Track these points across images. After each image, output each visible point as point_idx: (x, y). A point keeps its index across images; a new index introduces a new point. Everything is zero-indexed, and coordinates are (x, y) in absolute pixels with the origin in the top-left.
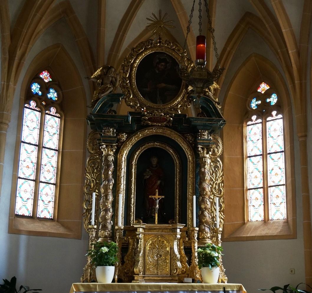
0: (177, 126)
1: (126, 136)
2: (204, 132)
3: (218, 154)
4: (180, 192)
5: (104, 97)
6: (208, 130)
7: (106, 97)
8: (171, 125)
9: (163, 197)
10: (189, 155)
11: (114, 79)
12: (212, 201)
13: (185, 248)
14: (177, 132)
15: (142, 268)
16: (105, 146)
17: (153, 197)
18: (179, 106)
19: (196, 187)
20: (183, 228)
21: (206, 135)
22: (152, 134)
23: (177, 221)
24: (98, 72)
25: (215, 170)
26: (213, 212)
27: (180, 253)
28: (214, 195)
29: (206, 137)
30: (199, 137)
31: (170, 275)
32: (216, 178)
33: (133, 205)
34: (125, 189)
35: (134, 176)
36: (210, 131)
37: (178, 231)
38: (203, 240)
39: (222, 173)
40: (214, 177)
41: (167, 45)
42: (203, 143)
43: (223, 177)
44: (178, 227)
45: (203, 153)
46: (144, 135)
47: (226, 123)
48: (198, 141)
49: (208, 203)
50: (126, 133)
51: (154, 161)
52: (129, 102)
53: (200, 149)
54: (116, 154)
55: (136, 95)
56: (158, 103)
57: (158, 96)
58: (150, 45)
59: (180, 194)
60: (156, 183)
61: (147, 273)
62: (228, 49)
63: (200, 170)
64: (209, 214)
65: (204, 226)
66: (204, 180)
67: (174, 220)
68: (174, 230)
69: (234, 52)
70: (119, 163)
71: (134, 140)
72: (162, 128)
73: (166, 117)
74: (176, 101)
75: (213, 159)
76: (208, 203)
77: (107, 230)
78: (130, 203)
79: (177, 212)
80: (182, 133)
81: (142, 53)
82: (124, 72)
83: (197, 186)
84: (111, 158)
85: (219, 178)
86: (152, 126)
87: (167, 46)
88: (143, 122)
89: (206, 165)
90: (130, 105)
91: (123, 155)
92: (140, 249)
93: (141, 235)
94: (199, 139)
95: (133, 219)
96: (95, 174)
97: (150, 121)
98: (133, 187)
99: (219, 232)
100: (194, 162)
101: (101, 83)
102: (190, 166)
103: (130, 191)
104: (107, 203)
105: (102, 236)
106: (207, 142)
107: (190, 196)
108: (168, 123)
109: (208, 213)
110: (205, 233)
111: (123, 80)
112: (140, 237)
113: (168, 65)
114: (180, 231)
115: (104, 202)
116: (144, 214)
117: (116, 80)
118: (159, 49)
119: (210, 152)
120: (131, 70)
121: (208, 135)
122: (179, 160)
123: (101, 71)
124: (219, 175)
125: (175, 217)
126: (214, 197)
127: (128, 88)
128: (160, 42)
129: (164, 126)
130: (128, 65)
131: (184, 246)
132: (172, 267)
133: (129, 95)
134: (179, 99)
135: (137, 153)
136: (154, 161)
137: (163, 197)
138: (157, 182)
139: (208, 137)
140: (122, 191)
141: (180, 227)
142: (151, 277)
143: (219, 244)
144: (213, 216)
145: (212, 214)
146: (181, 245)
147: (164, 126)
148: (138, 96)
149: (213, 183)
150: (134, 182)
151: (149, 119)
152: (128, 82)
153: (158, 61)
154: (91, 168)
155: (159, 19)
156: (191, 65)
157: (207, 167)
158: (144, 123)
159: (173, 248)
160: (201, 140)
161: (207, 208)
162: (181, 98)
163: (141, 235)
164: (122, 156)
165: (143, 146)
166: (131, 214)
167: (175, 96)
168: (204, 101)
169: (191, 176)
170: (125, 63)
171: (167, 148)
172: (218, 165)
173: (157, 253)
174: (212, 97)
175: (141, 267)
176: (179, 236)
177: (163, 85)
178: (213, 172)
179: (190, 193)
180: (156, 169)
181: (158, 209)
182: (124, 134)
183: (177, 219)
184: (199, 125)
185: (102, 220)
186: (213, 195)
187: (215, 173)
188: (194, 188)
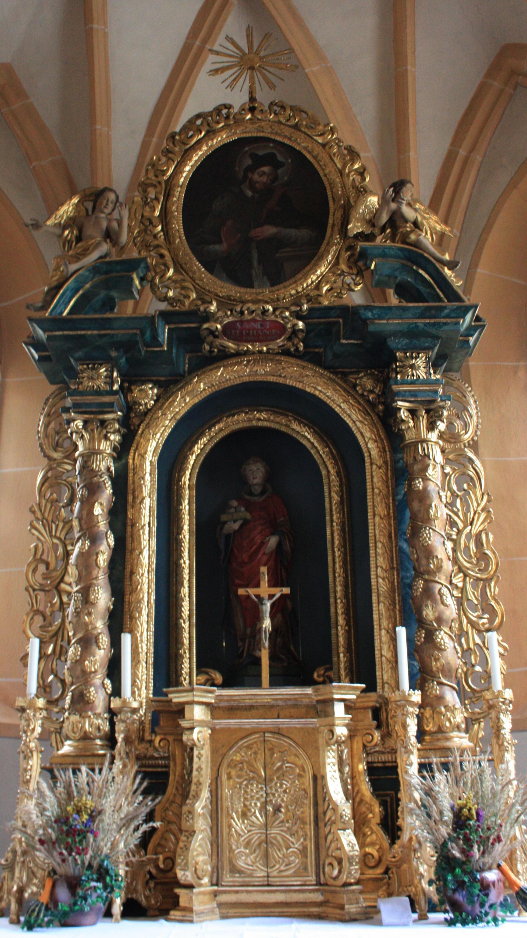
0: (322, 350)
1: (155, 391)
2: (412, 358)
3: (466, 436)
4: (345, 571)
5: (82, 275)
6: (425, 349)
7: (87, 273)
8: (301, 348)
9: (286, 590)
10: (370, 439)
11: (115, 224)
12: (460, 595)
13: (371, 770)
14: (326, 368)
15: (206, 857)
16: (80, 424)
17: (252, 592)
18: (325, 289)
19: (401, 551)
20: (358, 697)
21: (420, 367)
22: (238, 382)
23: (343, 672)
24: (67, 209)
25: (460, 488)
26: (467, 633)
27: (351, 794)
28: (466, 575)
29: (422, 373)
30: (397, 373)
31: (319, 883)
32: (465, 515)
33: (190, 620)
34: (154, 566)
35: (189, 525)
36: (433, 354)
37: (339, 709)
38: (440, 736)
39: (486, 498)
40: (460, 514)
41: (276, 114)
42: (413, 394)
43: (489, 512)
44: (336, 696)
45: (416, 426)
46: (213, 385)
47: (484, 326)
48: (395, 388)
49: (449, 601)
50: (156, 384)
51: (256, 472)
52: (165, 290)
53: (404, 414)
54: (121, 452)
55: (184, 266)
56: (256, 284)
57: (255, 263)
58: (223, 119)
59: (346, 578)
60: (263, 544)
61: (227, 878)
62: (462, 153)
63: (410, 486)
64: (453, 640)
65: (440, 684)
66: (428, 520)
67: (331, 669)
68: (323, 708)
69: (479, 158)
70: (134, 482)
71: (182, 403)
72: (272, 360)
73: (283, 318)
74: (314, 273)
75: (450, 453)
76: (449, 601)
77: (90, 713)
78: (177, 614)
79: (341, 640)
80: (339, 370)
81: (199, 142)
82: (146, 203)
83: (405, 546)
84: (105, 464)
85: (477, 515)
86: (238, 354)
87: (276, 119)
88: (208, 344)
89: (431, 467)
90: (165, 299)
91: (145, 453)
92: (199, 783)
93: (200, 732)
94: (396, 382)
95: (191, 668)
96: (61, 525)
97: (230, 338)
98: (187, 562)
99: (504, 707)
100: (385, 462)
101: (74, 239)
102: (376, 478)
103: (177, 575)
104: (89, 614)
105: (71, 735)
106: (425, 391)
107: (380, 580)
108: (289, 339)
109: (450, 636)
110: (443, 709)
111: (142, 227)
112: (195, 738)
113: (280, 171)
114: (347, 712)
115: (78, 614)
116: (228, 658)
117: (120, 223)
118: (250, 127)
119: (439, 423)
120: (168, 196)
121: (427, 367)
122: (336, 464)
123: (77, 205)
124: (475, 504)
125: (335, 659)
126: (464, 581)
127: (158, 246)
128: (252, 110)
129: (278, 354)
130: (160, 183)
131: (368, 763)
132: (323, 855)
133: (163, 268)
134: (322, 270)
135: (197, 449)
136: (256, 472)
137: (286, 590)
138: (269, 541)
139: (428, 373)
140: (146, 574)
141: (345, 692)
142: (242, 891)
143: (506, 754)
144: (465, 646)
145: (463, 640)
146: (355, 761)
147: (278, 354)
148: (192, 267)
149: (459, 532)
150: (189, 543)
151: (228, 331)
152: (159, 228)
153: (249, 162)
154: (49, 506)
155: (246, 51)
156: (352, 165)
157: (434, 473)
158: (211, 345)
159: (324, 777)
160: (404, 382)
161: (445, 617)
162: (329, 264)
163: (196, 730)
164: (143, 457)
165: (214, 425)
166: (181, 651)
167: (309, 256)
168: (403, 265)
169: (381, 510)
170: (150, 176)
171: (295, 426)
172: (471, 473)
173: (263, 800)
174: (432, 249)
175: (204, 854)
176: (341, 731)
177: (270, 230)
178: (454, 496)
179: (379, 570)
180: (261, 499)
181: (270, 635)
182: (150, 386)
183: (342, 666)
184: (395, 334)
185: (72, 677)
186: (461, 575)
187: (461, 499)
188: (391, 551)
